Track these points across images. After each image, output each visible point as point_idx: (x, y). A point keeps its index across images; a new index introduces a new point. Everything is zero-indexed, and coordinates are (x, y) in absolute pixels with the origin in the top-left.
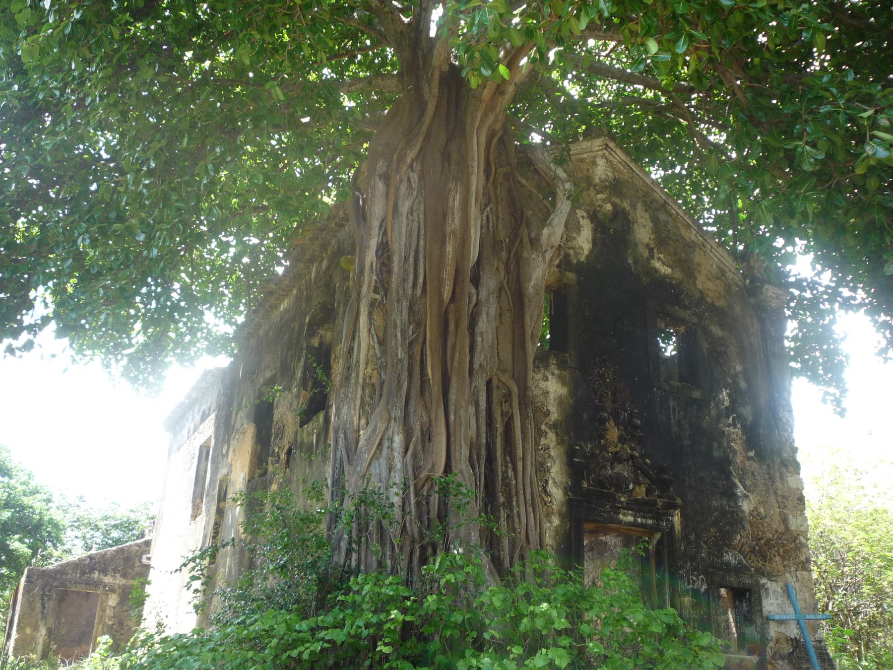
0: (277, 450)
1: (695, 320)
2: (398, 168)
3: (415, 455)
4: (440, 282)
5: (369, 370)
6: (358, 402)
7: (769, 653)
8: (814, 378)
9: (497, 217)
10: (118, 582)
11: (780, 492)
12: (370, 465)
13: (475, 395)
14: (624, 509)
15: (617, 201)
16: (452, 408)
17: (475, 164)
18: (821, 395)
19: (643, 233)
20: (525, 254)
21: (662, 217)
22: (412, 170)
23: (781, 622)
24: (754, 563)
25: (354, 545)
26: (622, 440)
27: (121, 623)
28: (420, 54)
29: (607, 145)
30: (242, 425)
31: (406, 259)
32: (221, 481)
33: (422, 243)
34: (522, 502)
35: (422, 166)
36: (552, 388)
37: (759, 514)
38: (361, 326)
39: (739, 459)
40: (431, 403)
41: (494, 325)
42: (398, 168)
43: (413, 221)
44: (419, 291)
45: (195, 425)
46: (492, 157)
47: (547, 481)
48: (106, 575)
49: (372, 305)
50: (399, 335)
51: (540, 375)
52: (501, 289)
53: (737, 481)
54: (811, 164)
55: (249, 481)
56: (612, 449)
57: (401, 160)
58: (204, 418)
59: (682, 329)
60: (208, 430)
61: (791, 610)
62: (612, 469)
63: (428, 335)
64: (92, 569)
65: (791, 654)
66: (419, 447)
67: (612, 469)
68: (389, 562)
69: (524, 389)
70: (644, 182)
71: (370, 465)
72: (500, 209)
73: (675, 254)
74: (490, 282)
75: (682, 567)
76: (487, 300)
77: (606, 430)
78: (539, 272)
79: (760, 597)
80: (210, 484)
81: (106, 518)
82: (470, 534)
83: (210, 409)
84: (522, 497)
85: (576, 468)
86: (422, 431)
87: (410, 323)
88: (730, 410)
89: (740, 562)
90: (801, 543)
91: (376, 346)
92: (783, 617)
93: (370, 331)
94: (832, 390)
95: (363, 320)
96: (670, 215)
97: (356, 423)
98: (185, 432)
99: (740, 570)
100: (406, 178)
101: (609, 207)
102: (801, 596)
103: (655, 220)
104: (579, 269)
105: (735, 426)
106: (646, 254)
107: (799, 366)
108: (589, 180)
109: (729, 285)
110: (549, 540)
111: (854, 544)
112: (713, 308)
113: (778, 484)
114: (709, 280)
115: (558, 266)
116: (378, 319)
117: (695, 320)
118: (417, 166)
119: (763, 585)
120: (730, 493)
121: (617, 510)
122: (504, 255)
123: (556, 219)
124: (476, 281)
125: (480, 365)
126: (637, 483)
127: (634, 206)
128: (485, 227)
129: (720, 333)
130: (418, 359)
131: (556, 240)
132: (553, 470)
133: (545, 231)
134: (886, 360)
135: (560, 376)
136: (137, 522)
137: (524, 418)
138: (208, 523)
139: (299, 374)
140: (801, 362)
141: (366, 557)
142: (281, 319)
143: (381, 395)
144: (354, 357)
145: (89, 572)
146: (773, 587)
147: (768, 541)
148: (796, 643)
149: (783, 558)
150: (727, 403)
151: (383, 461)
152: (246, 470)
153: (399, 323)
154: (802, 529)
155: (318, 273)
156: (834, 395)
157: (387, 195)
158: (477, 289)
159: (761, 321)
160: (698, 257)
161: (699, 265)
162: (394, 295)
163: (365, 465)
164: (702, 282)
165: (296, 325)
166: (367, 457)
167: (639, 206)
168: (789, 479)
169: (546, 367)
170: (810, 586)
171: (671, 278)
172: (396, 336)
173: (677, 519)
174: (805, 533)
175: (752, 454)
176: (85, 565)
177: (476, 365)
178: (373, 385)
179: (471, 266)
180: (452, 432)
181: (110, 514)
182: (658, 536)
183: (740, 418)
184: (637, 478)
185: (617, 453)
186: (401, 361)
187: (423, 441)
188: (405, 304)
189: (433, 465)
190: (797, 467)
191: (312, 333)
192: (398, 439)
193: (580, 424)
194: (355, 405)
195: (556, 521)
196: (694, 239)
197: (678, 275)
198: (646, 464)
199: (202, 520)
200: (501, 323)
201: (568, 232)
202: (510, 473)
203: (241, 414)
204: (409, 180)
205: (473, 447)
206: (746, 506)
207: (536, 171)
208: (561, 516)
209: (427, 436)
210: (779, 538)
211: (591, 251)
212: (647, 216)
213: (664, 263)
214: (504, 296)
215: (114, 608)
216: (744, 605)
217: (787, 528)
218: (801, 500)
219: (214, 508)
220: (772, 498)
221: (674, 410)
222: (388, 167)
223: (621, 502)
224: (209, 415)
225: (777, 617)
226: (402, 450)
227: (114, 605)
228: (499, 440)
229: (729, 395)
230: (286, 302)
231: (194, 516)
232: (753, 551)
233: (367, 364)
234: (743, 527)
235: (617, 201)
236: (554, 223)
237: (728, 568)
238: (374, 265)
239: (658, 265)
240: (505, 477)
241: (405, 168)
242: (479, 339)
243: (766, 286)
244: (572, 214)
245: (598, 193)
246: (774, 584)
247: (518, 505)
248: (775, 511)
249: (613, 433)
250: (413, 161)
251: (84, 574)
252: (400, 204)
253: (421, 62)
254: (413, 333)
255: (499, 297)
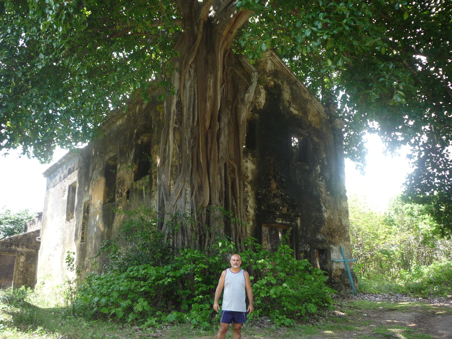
0: (120, 191)
1: (307, 135)
2: (185, 66)
3: (196, 197)
4: (205, 120)
5: (174, 159)
6: (169, 173)
7: (333, 275)
8: (353, 159)
9: (228, 89)
10: (24, 250)
11: (339, 209)
12: (176, 201)
13: (220, 169)
14: (278, 217)
15: (276, 80)
16: (211, 176)
17: (220, 66)
18: (355, 165)
19: (287, 96)
20: (239, 107)
21: (295, 88)
22: (191, 68)
23: (338, 263)
24: (328, 239)
25: (171, 236)
26: (277, 188)
27: (27, 269)
28: (193, 11)
29: (272, 54)
30: (97, 177)
31: (189, 109)
32: (85, 203)
33: (196, 102)
34: (239, 216)
35: (196, 66)
36: (249, 166)
37: (331, 218)
38: (170, 139)
39: (323, 195)
40: (202, 174)
41: (227, 139)
42: (185, 66)
43: (191, 91)
44: (195, 124)
45: (64, 175)
46: (225, 62)
47: (247, 207)
48: (18, 247)
49: (175, 129)
50: (187, 144)
51: (244, 160)
52: (229, 122)
53: (323, 205)
54: (374, 100)
55: (104, 204)
56: (273, 192)
57: (186, 63)
58: (70, 172)
59: (301, 138)
60: (74, 178)
61: (342, 257)
62: (273, 200)
63: (200, 144)
64: (11, 245)
65: (341, 275)
66: (198, 193)
67: (273, 200)
68: (186, 243)
69: (239, 167)
70: (287, 71)
71: (176, 201)
72: (229, 86)
73: (300, 105)
74: (225, 120)
75: (300, 241)
76: (224, 127)
77: (271, 184)
78: (244, 114)
79: (330, 252)
80: (78, 205)
81: (6, 219)
82: (220, 230)
83: (74, 168)
84: (239, 214)
85: (259, 201)
86: (198, 186)
87: (191, 138)
88: (321, 174)
89: (323, 239)
90: (346, 230)
91: (177, 148)
92: (339, 260)
93: (174, 142)
94: (360, 164)
95: (171, 136)
96: (298, 87)
97: (168, 183)
98: (58, 178)
99: (323, 242)
100: (188, 71)
101: (272, 83)
102: (346, 252)
103: (291, 89)
104: (260, 112)
105: (322, 181)
106: (288, 105)
107: (347, 153)
108: (264, 70)
109: (321, 119)
110: (248, 232)
111: (363, 228)
112: (315, 129)
113: (339, 206)
114: (313, 116)
115: (252, 111)
116: (178, 137)
117: (307, 135)
118: (193, 66)
119: (332, 248)
120: (319, 210)
121: (275, 218)
122: (230, 107)
123: (251, 89)
124: (219, 120)
125: (222, 157)
126: (283, 206)
127: (283, 83)
128: (222, 93)
129: (317, 140)
130: (196, 154)
131: (251, 99)
132: (250, 201)
133: (247, 95)
134: (386, 155)
135: (252, 160)
136: (22, 220)
137: (240, 180)
138: (78, 223)
139: (132, 157)
140: (348, 151)
141: (177, 240)
142: (118, 129)
143: (180, 170)
144: (167, 153)
145: (10, 246)
146: (335, 248)
147: (334, 229)
148: (343, 271)
149: (339, 236)
150: (319, 171)
151: (182, 199)
152: (102, 199)
153: (187, 138)
154: (347, 224)
155: (140, 110)
156: (361, 166)
157: (180, 78)
158: (219, 122)
159: (334, 135)
160: (309, 106)
161: (309, 109)
162: (185, 125)
163: (174, 201)
164: (311, 118)
165: (128, 133)
166: (175, 198)
167: (285, 82)
168: (343, 203)
169: (247, 157)
170: (350, 248)
171: (298, 116)
172: (186, 144)
173: (299, 222)
174: (348, 226)
175: (329, 193)
176: (8, 243)
177: (220, 157)
178: (176, 166)
179: (209, 108)
180: (211, 187)
181: (8, 216)
182: (291, 228)
183: (324, 178)
184: (283, 204)
185: (275, 194)
186: (188, 155)
187: (199, 190)
188: (189, 129)
189: (204, 201)
190: (346, 198)
191: (138, 137)
192: (189, 189)
193: (261, 182)
194: (168, 175)
195: (251, 223)
196: (307, 98)
197: (301, 114)
198: (287, 198)
199: (73, 222)
200: (230, 138)
201: (256, 96)
202: (234, 204)
203: (95, 172)
204: (189, 72)
205: (221, 194)
206: (326, 215)
207: (243, 67)
208: (253, 220)
209: (201, 188)
210: (338, 228)
211: (265, 104)
212: (288, 87)
213: (295, 109)
214: (230, 125)
215: (23, 262)
216: (324, 256)
217: (341, 224)
218: (347, 212)
219: (81, 216)
220: (336, 211)
221: (298, 174)
222: (180, 66)
223: (277, 215)
224: (73, 171)
225: (337, 261)
226: (190, 195)
227: (23, 261)
228: (230, 190)
229: (320, 168)
230: (120, 121)
231: (68, 220)
232: (328, 234)
233: (173, 157)
234: (324, 224)
235: (276, 80)
236: (250, 91)
237: (318, 241)
238: (175, 112)
239: (292, 110)
240: (232, 206)
241: (188, 67)
242: (221, 145)
243: (337, 119)
244: (257, 87)
245: (268, 77)
246: (336, 247)
247: (238, 217)
248: (337, 217)
249: (274, 185)
250: (191, 63)
251: (8, 247)
252: (186, 83)
253: (193, 14)
254: (193, 143)
255: (229, 126)
